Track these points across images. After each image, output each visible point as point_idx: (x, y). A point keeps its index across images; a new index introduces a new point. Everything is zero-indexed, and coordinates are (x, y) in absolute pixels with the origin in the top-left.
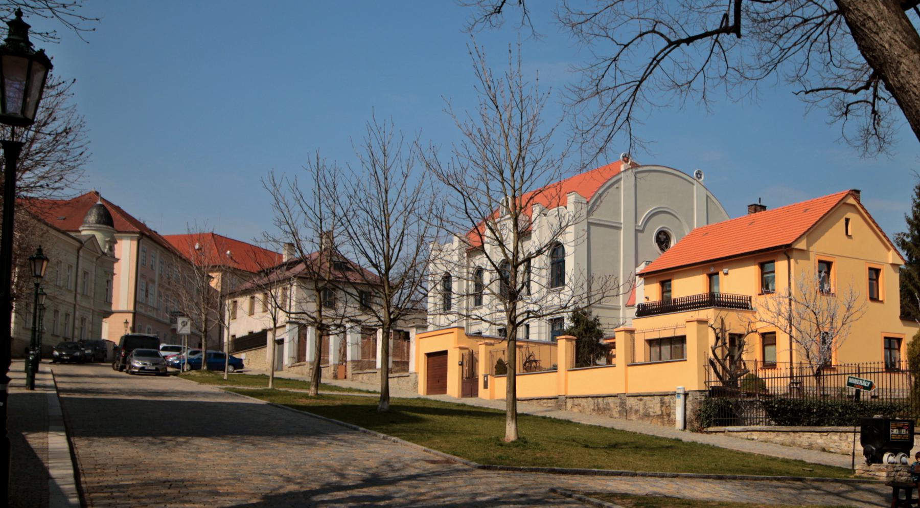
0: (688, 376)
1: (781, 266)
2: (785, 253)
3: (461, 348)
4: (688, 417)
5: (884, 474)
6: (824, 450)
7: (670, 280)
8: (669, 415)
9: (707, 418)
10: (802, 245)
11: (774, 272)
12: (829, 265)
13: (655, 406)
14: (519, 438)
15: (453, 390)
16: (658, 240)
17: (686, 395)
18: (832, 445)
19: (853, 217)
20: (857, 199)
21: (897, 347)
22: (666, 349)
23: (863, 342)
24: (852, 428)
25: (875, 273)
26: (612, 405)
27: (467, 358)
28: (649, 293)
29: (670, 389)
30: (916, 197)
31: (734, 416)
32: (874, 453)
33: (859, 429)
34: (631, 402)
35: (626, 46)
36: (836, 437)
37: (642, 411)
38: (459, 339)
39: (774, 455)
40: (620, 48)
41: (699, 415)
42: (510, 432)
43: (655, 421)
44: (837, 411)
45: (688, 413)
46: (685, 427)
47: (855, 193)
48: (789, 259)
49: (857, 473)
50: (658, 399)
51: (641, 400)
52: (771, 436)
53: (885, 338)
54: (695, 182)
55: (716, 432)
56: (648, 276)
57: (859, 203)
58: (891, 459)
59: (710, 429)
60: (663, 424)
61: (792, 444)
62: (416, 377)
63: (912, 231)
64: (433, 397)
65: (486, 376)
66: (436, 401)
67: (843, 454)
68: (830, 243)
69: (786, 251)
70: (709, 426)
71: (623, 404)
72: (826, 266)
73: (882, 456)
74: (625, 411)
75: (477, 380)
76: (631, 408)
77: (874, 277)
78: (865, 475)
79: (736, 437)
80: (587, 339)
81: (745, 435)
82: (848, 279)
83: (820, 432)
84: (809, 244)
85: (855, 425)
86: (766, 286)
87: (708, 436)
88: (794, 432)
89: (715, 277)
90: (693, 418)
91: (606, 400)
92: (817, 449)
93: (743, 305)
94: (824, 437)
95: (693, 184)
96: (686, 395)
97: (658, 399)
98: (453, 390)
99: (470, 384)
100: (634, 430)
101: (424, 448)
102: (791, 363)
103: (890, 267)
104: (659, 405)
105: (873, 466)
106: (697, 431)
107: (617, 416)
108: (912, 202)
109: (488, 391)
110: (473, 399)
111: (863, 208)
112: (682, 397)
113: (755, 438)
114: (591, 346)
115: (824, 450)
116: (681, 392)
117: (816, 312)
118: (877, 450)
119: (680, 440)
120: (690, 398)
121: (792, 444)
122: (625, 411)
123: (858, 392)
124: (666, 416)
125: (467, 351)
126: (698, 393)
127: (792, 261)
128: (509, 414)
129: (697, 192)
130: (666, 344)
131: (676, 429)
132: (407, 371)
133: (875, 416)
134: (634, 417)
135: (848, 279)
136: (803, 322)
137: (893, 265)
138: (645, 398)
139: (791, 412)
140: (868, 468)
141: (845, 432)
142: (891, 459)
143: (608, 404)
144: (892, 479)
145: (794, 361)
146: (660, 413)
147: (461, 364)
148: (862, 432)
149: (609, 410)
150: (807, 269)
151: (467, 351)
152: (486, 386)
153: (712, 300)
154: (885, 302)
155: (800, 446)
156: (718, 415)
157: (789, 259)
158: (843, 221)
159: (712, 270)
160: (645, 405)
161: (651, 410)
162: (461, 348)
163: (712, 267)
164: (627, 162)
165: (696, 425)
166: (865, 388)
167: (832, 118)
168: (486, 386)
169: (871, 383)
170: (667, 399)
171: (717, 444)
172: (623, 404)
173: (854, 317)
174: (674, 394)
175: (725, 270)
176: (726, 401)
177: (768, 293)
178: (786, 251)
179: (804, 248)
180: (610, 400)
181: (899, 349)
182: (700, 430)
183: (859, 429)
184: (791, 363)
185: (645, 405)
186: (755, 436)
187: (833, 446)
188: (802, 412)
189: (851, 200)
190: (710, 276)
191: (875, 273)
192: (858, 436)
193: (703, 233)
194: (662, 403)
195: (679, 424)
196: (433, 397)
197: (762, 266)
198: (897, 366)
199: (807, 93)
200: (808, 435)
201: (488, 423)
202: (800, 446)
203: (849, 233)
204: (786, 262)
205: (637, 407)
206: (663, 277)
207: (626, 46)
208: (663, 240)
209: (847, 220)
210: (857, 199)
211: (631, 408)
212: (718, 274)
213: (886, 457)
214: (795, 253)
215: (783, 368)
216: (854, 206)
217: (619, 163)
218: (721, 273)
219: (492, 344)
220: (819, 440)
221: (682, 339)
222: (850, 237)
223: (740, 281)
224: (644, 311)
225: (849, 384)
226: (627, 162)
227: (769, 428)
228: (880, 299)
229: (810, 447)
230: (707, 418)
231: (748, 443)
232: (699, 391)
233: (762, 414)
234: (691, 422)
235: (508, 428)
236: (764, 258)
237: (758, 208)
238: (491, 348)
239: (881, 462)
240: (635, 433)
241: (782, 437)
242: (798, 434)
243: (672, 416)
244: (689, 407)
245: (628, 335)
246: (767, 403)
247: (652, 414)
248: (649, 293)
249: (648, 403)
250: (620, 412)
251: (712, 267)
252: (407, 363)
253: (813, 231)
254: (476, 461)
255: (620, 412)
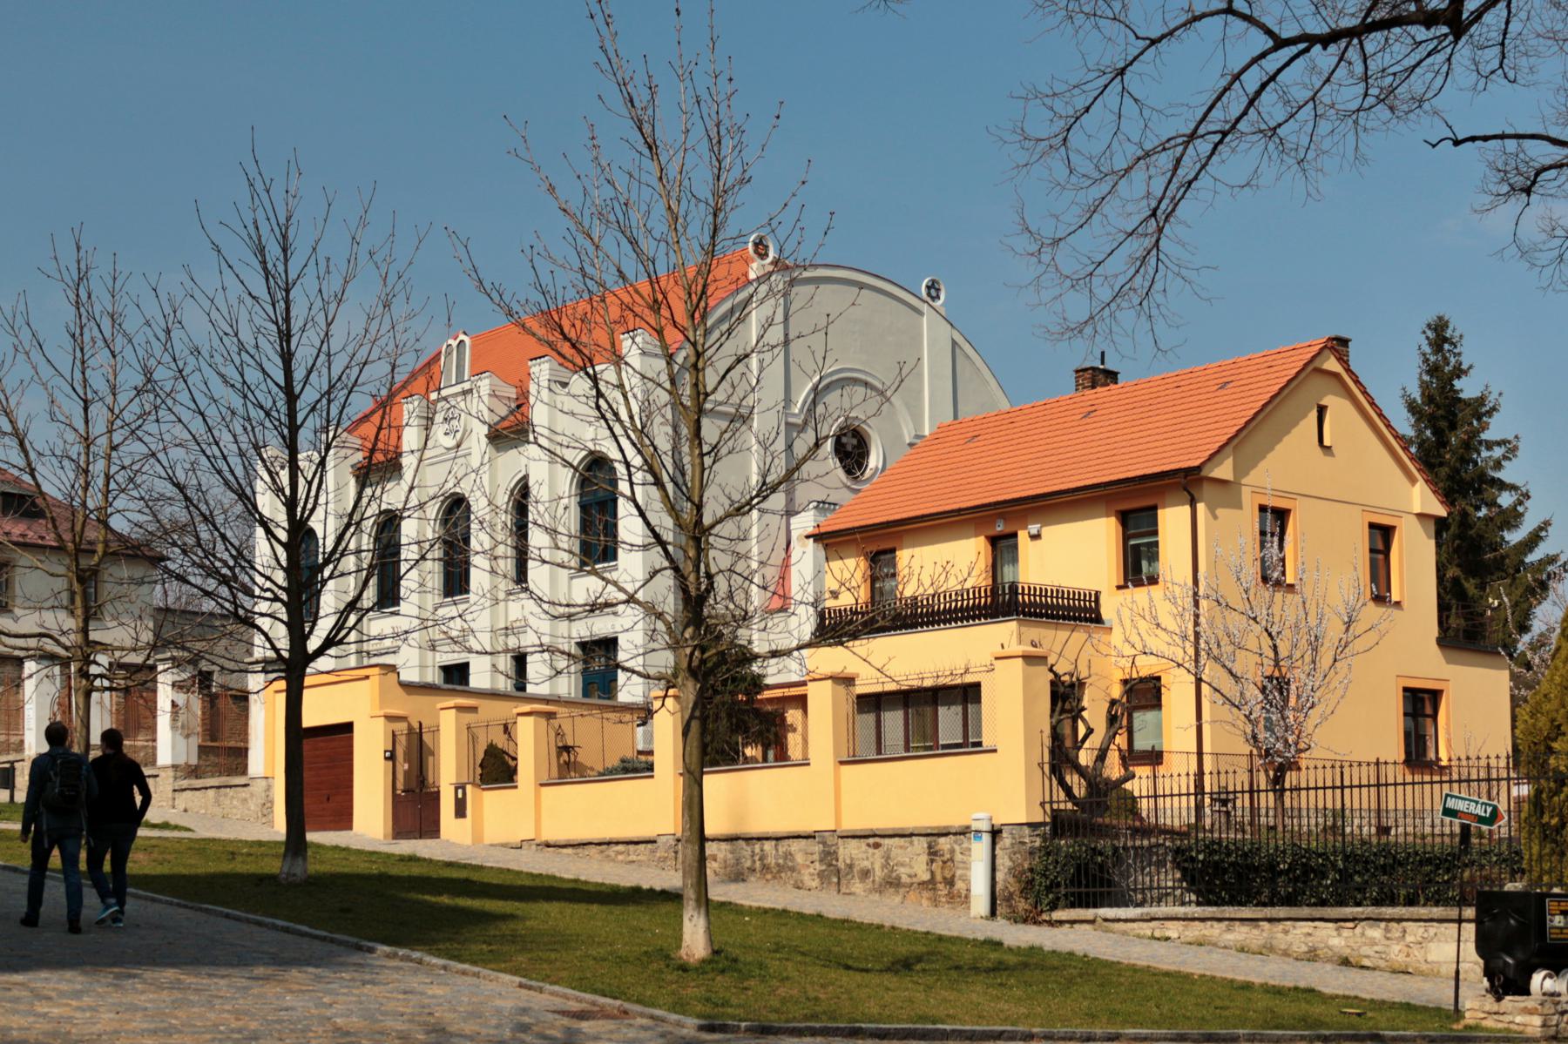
0: (996, 787)
1: (1173, 521)
2: (1185, 489)
3: (390, 718)
4: (999, 887)
5: (1537, 1021)
6: (1345, 962)
7: (893, 551)
8: (950, 882)
9: (1049, 889)
10: (1224, 470)
11: (1155, 533)
12: (1281, 515)
13: (914, 861)
14: (716, 952)
15: (370, 820)
16: (840, 450)
17: (995, 833)
18: (1366, 950)
19: (1337, 406)
20: (1343, 360)
21: (1429, 710)
22: (894, 720)
23: (1388, 701)
24: (1453, 912)
25: (1382, 535)
26: (800, 859)
27: (402, 740)
28: (847, 581)
29: (956, 822)
30: (1428, 350)
31: (1110, 883)
32: (1511, 974)
33: (1470, 912)
34: (851, 851)
35: (1153, 42)
36: (1376, 932)
37: (879, 874)
38: (383, 698)
39: (1240, 978)
40: (1142, 44)
41: (1031, 882)
42: (694, 938)
43: (912, 895)
44: (1334, 865)
45: (1000, 876)
46: (993, 913)
47: (1339, 345)
48: (1193, 503)
49: (1470, 1018)
50: (921, 844)
51: (877, 846)
52: (1214, 931)
53: (1405, 690)
54: (925, 308)
55: (1073, 922)
56: (831, 541)
57: (1348, 370)
58: (1549, 985)
59: (1058, 915)
60: (935, 902)
61: (1267, 950)
62: (269, 788)
63: (1420, 432)
64: (406, 847)
65: (460, 787)
66: (412, 859)
67: (1394, 972)
68: (1286, 466)
69: (1186, 483)
70: (1054, 906)
71: (829, 856)
72: (1276, 518)
73: (1530, 978)
74: (834, 872)
75: (436, 797)
76: (851, 866)
77: (1380, 546)
78: (1489, 1023)
79: (1124, 933)
80: (727, 698)
81: (1146, 929)
82: (1326, 556)
83: (1336, 921)
84: (1241, 470)
85: (1462, 902)
86: (1138, 564)
87: (1055, 931)
88: (1270, 920)
89: (1003, 543)
90: (1014, 887)
91: (784, 846)
92: (1329, 961)
93: (1081, 612)
94: (1346, 933)
95: (920, 313)
96: (995, 833)
97: (921, 844)
98: (370, 820)
99: (416, 806)
100: (876, 921)
101: (517, 979)
102: (1200, 753)
103: (1414, 519)
104: (924, 858)
105: (1509, 1002)
106: (1025, 921)
107: (815, 883)
108: (1419, 360)
109: (467, 822)
110: (429, 842)
111: (1357, 382)
112: (986, 838)
113: (1174, 935)
114: (735, 716)
115: (1345, 962)
116: (985, 826)
117: (1274, 631)
118: (1518, 963)
119: (1000, 944)
120: (1006, 840)
121: (1267, 950)
122: (834, 872)
123: (1465, 829)
124: (944, 884)
125: (402, 726)
126: (1027, 830)
127: (1201, 507)
128: (690, 894)
129: (931, 333)
130: (892, 707)
131: (972, 915)
132: (244, 772)
133: (1509, 887)
134: (858, 887)
135: (1326, 556)
136: (1240, 654)
137: (1421, 516)
138: (887, 841)
139: (1232, 873)
140: (1495, 1007)
141: (1400, 920)
142: (1549, 985)
143: (788, 855)
144: (1552, 1031)
145: (1207, 748)
146: (926, 877)
147: (391, 757)
148: (1478, 921)
149: (793, 869)
150: (1232, 532)
151: (402, 726)
152: (460, 811)
153: (1002, 602)
154: (1405, 605)
155: (1286, 954)
156: (1075, 881)
157: (1193, 503)
158: (1314, 414)
159: (1000, 528)
160: (887, 858)
161: (902, 871)
162: (390, 718)
163: (1001, 523)
164: (763, 256)
165: (1022, 905)
166: (1481, 820)
167: (1488, 199)
168: (460, 811)
169: (1495, 809)
170: (944, 843)
171: (1079, 949)
172: (829, 856)
173: (1358, 645)
174: (964, 832)
175: (1034, 529)
176: (1084, 850)
177: (1138, 583)
178: (1186, 483)
179: (1229, 476)
180: (795, 846)
181: (1435, 717)
182: (1030, 919)
183: (1470, 912)
184: (1200, 753)
185: (887, 858)
186: (1173, 929)
187: (1368, 954)
188: (1256, 869)
189: (1332, 364)
190: (994, 541)
191: (1382, 535)
192: (1470, 930)
193: (962, 432)
194: (933, 853)
195: (980, 901)
196: (406, 847)
197: (1124, 518)
198: (1431, 755)
199: (1457, 143)
200: (1306, 927)
201: (637, 916)
202: (1286, 954)
203: (1327, 442)
204: (1187, 509)
205: (866, 864)
206: (878, 543)
207: (1153, 42)
208: (852, 450)
209: (1322, 410)
210: (1343, 360)
211: (851, 866)
212: (1015, 535)
213: (1537, 979)
214: (1207, 490)
215: (1178, 767)
216: (1336, 375)
217: (747, 262)
218: (1022, 536)
219: (474, 709)
220: (1332, 938)
221: (968, 694)
222: (1327, 449)
223: (1068, 556)
224: (834, 629)
225: (1448, 812)
226: (763, 256)
227: (1180, 910)
228: (1395, 597)
229: (1312, 956)
230: (1049, 889)
231: (1160, 948)
232: (1029, 825)
233: (1169, 878)
234: (1009, 898)
235: (687, 926)
236: (1134, 506)
237: (1099, 376)
238: (469, 718)
239: (1526, 991)
240: (880, 927)
241: (1241, 933)
242: (1281, 926)
243: (959, 885)
244: (1004, 862)
245: (841, 689)
246: (1178, 851)
247: (905, 879)
248: (847, 581)
249: (894, 852)
250: (821, 875)
251: (1001, 523)
252: (242, 753)
253: (1250, 437)
254: (698, 1017)
255: (821, 875)
